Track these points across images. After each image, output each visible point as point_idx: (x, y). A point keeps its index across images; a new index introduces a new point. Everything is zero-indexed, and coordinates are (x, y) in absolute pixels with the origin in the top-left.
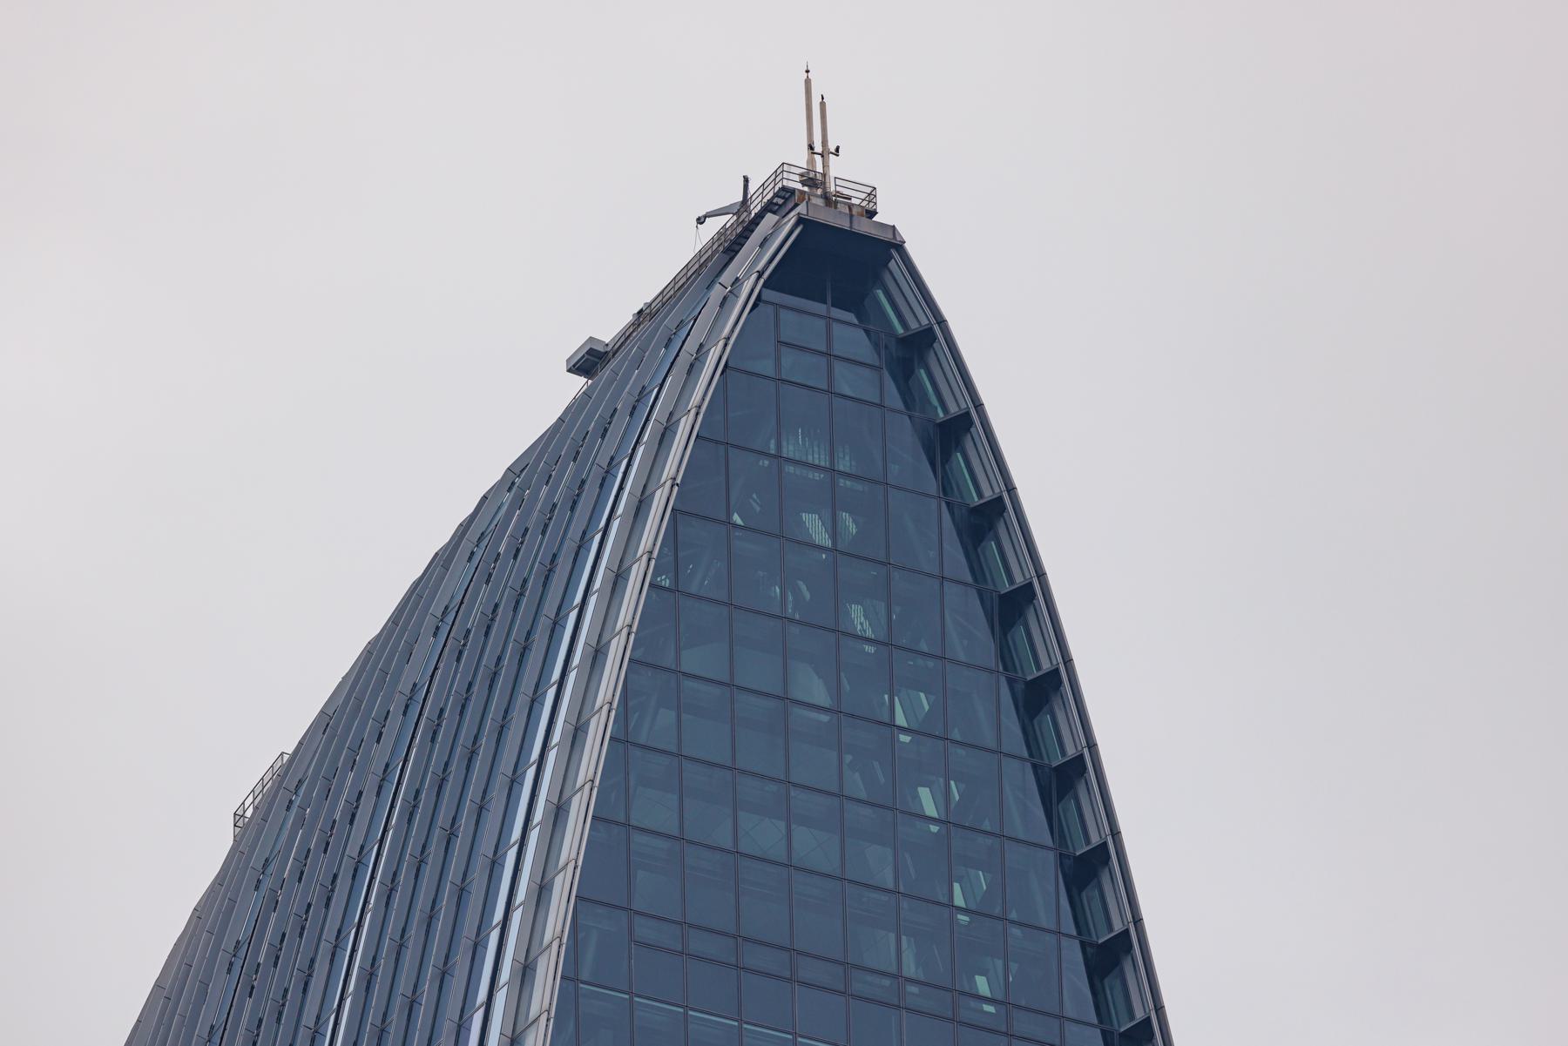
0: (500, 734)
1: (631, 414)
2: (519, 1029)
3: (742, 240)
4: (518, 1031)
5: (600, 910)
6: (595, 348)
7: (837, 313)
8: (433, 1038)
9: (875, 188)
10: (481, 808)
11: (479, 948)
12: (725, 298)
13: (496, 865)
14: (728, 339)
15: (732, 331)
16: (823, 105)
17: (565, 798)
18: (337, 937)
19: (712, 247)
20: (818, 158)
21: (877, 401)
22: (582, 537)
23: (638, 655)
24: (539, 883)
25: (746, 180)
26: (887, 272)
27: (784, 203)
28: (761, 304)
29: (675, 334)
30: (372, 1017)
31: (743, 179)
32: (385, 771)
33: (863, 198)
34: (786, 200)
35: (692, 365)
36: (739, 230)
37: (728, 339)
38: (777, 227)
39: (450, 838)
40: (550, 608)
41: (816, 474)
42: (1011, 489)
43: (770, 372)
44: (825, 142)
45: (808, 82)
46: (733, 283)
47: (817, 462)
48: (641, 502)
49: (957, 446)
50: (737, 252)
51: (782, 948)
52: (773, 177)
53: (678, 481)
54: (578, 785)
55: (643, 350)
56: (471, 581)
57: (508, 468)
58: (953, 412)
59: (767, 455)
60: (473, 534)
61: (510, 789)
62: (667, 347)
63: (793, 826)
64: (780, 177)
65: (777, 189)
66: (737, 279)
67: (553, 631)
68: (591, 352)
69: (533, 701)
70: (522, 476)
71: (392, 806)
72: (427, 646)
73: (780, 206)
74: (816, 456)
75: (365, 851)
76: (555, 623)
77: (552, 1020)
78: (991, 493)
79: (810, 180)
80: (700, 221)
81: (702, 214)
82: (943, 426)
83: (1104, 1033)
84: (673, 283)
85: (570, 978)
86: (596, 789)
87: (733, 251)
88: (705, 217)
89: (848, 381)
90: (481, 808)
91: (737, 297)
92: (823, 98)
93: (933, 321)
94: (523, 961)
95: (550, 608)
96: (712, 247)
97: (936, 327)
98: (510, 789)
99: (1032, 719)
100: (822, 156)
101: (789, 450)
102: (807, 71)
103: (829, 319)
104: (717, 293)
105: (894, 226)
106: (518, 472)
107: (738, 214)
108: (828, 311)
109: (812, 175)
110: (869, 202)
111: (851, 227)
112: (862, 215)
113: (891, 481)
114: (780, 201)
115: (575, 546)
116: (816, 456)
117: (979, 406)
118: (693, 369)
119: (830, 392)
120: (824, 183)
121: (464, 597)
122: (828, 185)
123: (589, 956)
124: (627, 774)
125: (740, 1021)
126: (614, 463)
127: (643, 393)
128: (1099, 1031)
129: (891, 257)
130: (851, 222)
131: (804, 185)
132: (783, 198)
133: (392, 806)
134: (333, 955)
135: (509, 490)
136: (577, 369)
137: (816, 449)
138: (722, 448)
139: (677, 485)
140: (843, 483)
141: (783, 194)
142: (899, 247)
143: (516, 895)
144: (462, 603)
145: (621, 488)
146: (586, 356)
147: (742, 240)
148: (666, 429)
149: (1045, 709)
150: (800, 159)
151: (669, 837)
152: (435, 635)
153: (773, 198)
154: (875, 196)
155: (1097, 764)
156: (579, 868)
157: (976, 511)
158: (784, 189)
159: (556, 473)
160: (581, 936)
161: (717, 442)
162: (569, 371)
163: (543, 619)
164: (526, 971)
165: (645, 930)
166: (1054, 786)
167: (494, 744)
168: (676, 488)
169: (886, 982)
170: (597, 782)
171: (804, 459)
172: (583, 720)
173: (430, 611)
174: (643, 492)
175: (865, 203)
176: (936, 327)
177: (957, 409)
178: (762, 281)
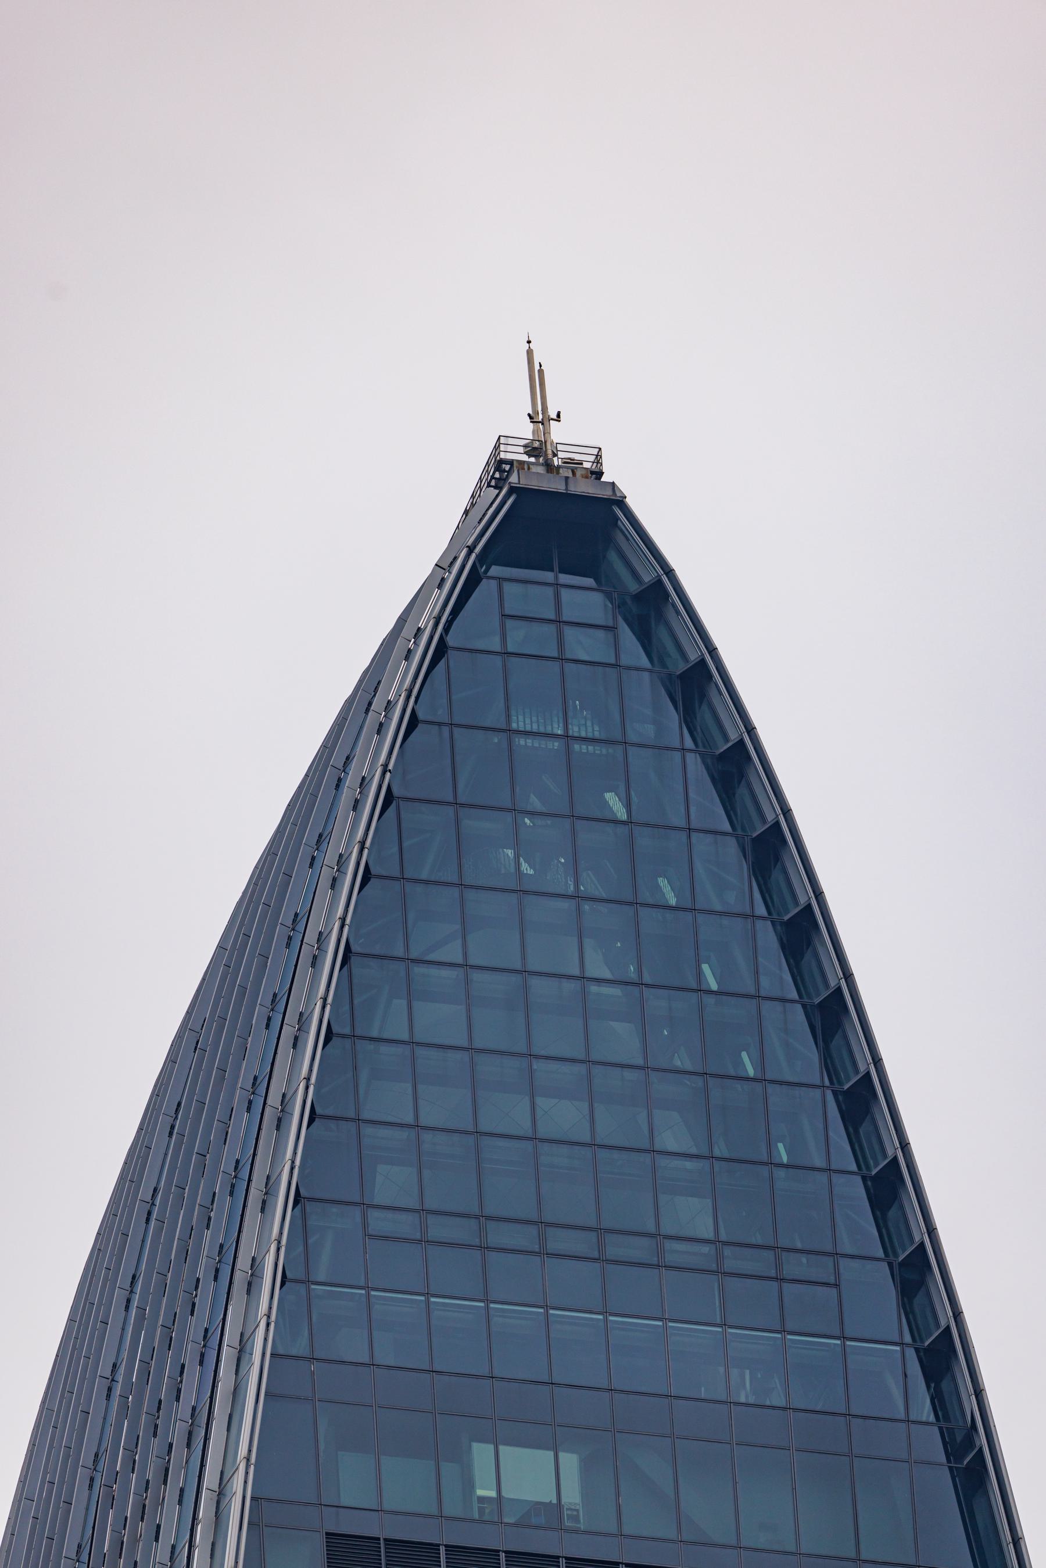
7: (565, 578)
21: (613, 661)
26: (618, 532)
41: (584, 747)
45: (530, 353)
47: (528, 728)
51: (528, 1222)
53: (390, 767)
59: (554, 736)
63: (596, 1105)
74: (590, 729)
79: (533, 450)
97: (665, 579)
100: (543, 424)
101: (519, 722)
102: (529, 342)
103: (557, 585)
105: (613, 483)
108: (556, 578)
109: (537, 444)
110: (597, 463)
111: (567, 489)
116: (528, 721)
119: (561, 659)
125: (487, 1301)
128: (886, 1263)
130: (567, 484)
131: (530, 456)
137: (556, 719)
142: (621, 503)
150: (526, 431)
155: (854, 994)
161: (440, 724)
165: (379, 1221)
169: (705, 1249)
176: (665, 579)
178: (473, 556)
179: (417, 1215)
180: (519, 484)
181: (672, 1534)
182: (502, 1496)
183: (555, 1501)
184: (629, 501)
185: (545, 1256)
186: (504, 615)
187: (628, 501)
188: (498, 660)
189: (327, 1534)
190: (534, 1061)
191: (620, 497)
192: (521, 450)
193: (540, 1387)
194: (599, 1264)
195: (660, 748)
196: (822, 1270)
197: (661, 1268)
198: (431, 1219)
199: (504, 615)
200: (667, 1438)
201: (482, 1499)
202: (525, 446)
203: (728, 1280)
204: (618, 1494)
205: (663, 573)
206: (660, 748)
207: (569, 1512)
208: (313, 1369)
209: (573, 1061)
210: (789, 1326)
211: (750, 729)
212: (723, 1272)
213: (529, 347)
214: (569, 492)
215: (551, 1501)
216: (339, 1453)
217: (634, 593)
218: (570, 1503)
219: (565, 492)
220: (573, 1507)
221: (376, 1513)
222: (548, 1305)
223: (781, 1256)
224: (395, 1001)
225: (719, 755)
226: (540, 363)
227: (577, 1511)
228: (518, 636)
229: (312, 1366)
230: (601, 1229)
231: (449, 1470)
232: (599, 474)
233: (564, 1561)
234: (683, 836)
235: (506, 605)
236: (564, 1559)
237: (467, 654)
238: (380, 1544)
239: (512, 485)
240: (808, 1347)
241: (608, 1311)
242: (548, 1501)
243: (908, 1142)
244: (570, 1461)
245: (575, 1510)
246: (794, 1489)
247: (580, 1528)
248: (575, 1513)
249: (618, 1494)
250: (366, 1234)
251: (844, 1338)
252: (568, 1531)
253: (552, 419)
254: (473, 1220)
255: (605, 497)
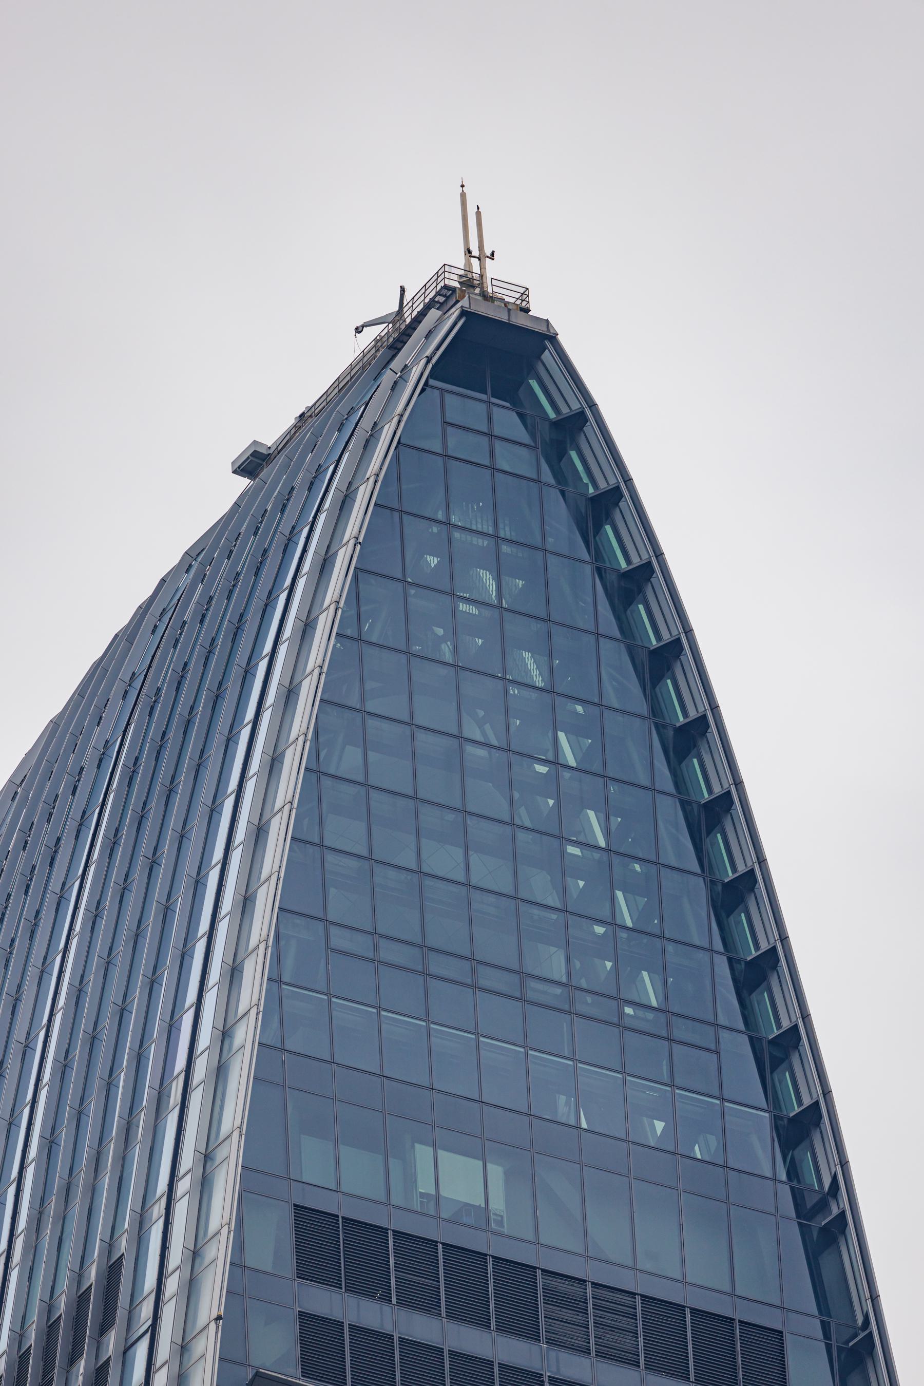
0: (197, 771)
1: (310, 489)
2: (230, 1022)
3: (405, 338)
4: (228, 1026)
5: (299, 921)
6: (257, 450)
8: (145, 1039)
9: (528, 289)
10: (182, 837)
11: (186, 957)
12: (395, 383)
13: (199, 884)
14: (401, 416)
15: (405, 409)
16: (478, 214)
17: (264, 820)
18: (44, 963)
19: (350, 373)
20: (475, 263)
22: (269, 597)
23: (326, 697)
24: (244, 895)
25: (403, 290)
27: (445, 301)
28: (428, 389)
29: (346, 419)
30: (84, 1025)
31: (399, 289)
32: (82, 817)
33: (517, 297)
34: (447, 298)
35: (367, 441)
36: (396, 335)
37: (401, 416)
38: (440, 322)
39: (152, 865)
40: (241, 658)
42: (659, 555)
43: (438, 448)
44: (481, 247)
45: (463, 196)
46: (403, 370)
48: (325, 560)
49: (607, 519)
50: (400, 350)
52: (435, 277)
53: (361, 540)
54: (277, 808)
55: (316, 435)
56: (158, 647)
57: (235, 503)
58: (602, 487)
60: (156, 610)
61: (210, 818)
62: (339, 430)
63: (471, 853)
64: (442, 277)
65: (439, 288)
66: (406, 366)
67: (244, 678)
68: (255, 454)
69: (228, 740)
70: (199, 559)
71: (92, 845)
72: (116, 711)
73: (442, 304)
75: (67, 887)
76: (246, 672)
77: (261, 1014)
78: (639, 560)
79: (468, 283)
80: (358, 330)
81: (360, 324)
82: (594, 500)
83: (751, 1039)
84: (337, 382)
85: (275, 980)
86: (294, 810)
87: (396, 348)
88: (363, 326)
89: (506, 458)
90: (182, 837)
91: (407, 382)
92: (478, 208)
93: (585, 405)
94: (231, 963)
95: (241, 658)
96: (350, 373)
98: (210, 818)
99: (680, 763)
100: (479, 260)
102: (462, 186)
104: (388, 378)
106: (194, 556)
107: (393, 322)
109: (470, 275)
110: (523, 301)
111: (509, 319)
112: (517, 310)
113: (548, 547)
114: (442, 299)
115: (262, 604)
117: (628, 481)
118: (369, 444)
119: (493, 468)
120: (481, 285)
121: (151, 662)
122: (485, 285)
123: (289, 964)
124: (320, 800)
125: (428, 1020)
126: (295, 531)
127: (320, 470)
129: (545, 348)
130: (509, 315)
132: (444, 296)
133: (92, 845)
134: (41, 978)
135: (187, 571)
136: (241, 470)
137: (479, 520)
138: (396, 514)
139: (360, 543)
140: (505, 548)
141: (444, 292)
142: (553, 338)
143: (221, 908)
144: (150, 666)
145: (305, 551)
146: (251, 458)
147: (405, 338)
148: (346, 496)
149: (694, 752)
151: (359, 857)
152: (124, 698)
153: (435, 296)
154: (528, 296)
156: (281, 879)
157: (626, 575)
158: (446, 287)
159: (210, 573)
160: (282, 943)
161: (392, 509)
162: (234, 472)
163: (235, 668)
164: (234, 973)
165: (340, 939)
166: (703, 822)
167: (163, 807)
168: (358, 547)
169: (558, 991)
170: (295, 804)
171: (468, 526)
172: (279, 751)
173: (119, 677)
174: (327, 552)
175: (519, 302)
176: (588, 411)
177: (606, 485)
178: (430, 366)
179: (371, 937)
180: (470, 308)
181: (580, 1250)
182: (441, 1195)
183: (483, 1205)
184: (561, 338)
185: (477, 989)
186: (445, 422)
187: (559, 337)
188: (440, 461)
189: (295, 1205)
190: (468, 817)
191: (553, 333)
192: (456, 277)
193: (471, 1104)
194: (521, 1003)
195: (574, 559)
196: (705, 1037)
197: (572, 1014)
198: (382, 942)
199: (445, 422)
200: (576, 1164)
201: (422, 1195)
202: (461, 276)
203: (627, 1034)
204: (535, 1208)
205: (587, 406)
206: (574, 559)
207: (495, 1217)
208: (283, 1058)
209: (500, 822)
210: (678, 1081)
211: (658, 554)
212: (623, 1026)
213: (463, 191)
214: (511, 322)
215: (480, 1205)
216: (301, 1135)
217: (553, 421)
218: (496, 1209)
219: (507, 321)
220: (498, 1213)
221: (335, 1193)
222: (479, 1032)
223: (672, 1019)
224: (349, 748)
225: (622, 573)
226: (478, 206)
227: (502, 1217)
228: (456, 442)
229: (283, 1056)
230: (474, 960)
231: (395, 1165)
232: (527, 310)
233: (491, 1259)
234: (592, 639)
235: (448, 414)
236: (491, 1257)
237: (415, 452)
238: (338, 1221)
239: (464, 309)
240: (345, 1011)
241: (528, 1045)
242: (478, 1205)
243: (787, 936)
244: (496, 1172)
245: (500, 1215)
246: (681, 1225)
247: (504, 1232)
248: (499, 1218)
249: (535, 1208)
250: (327, 947)
251: (723, 1099)
252: (494, 1233)
253: (488, 257)
254: (417, 949)
255: (541, 332)
